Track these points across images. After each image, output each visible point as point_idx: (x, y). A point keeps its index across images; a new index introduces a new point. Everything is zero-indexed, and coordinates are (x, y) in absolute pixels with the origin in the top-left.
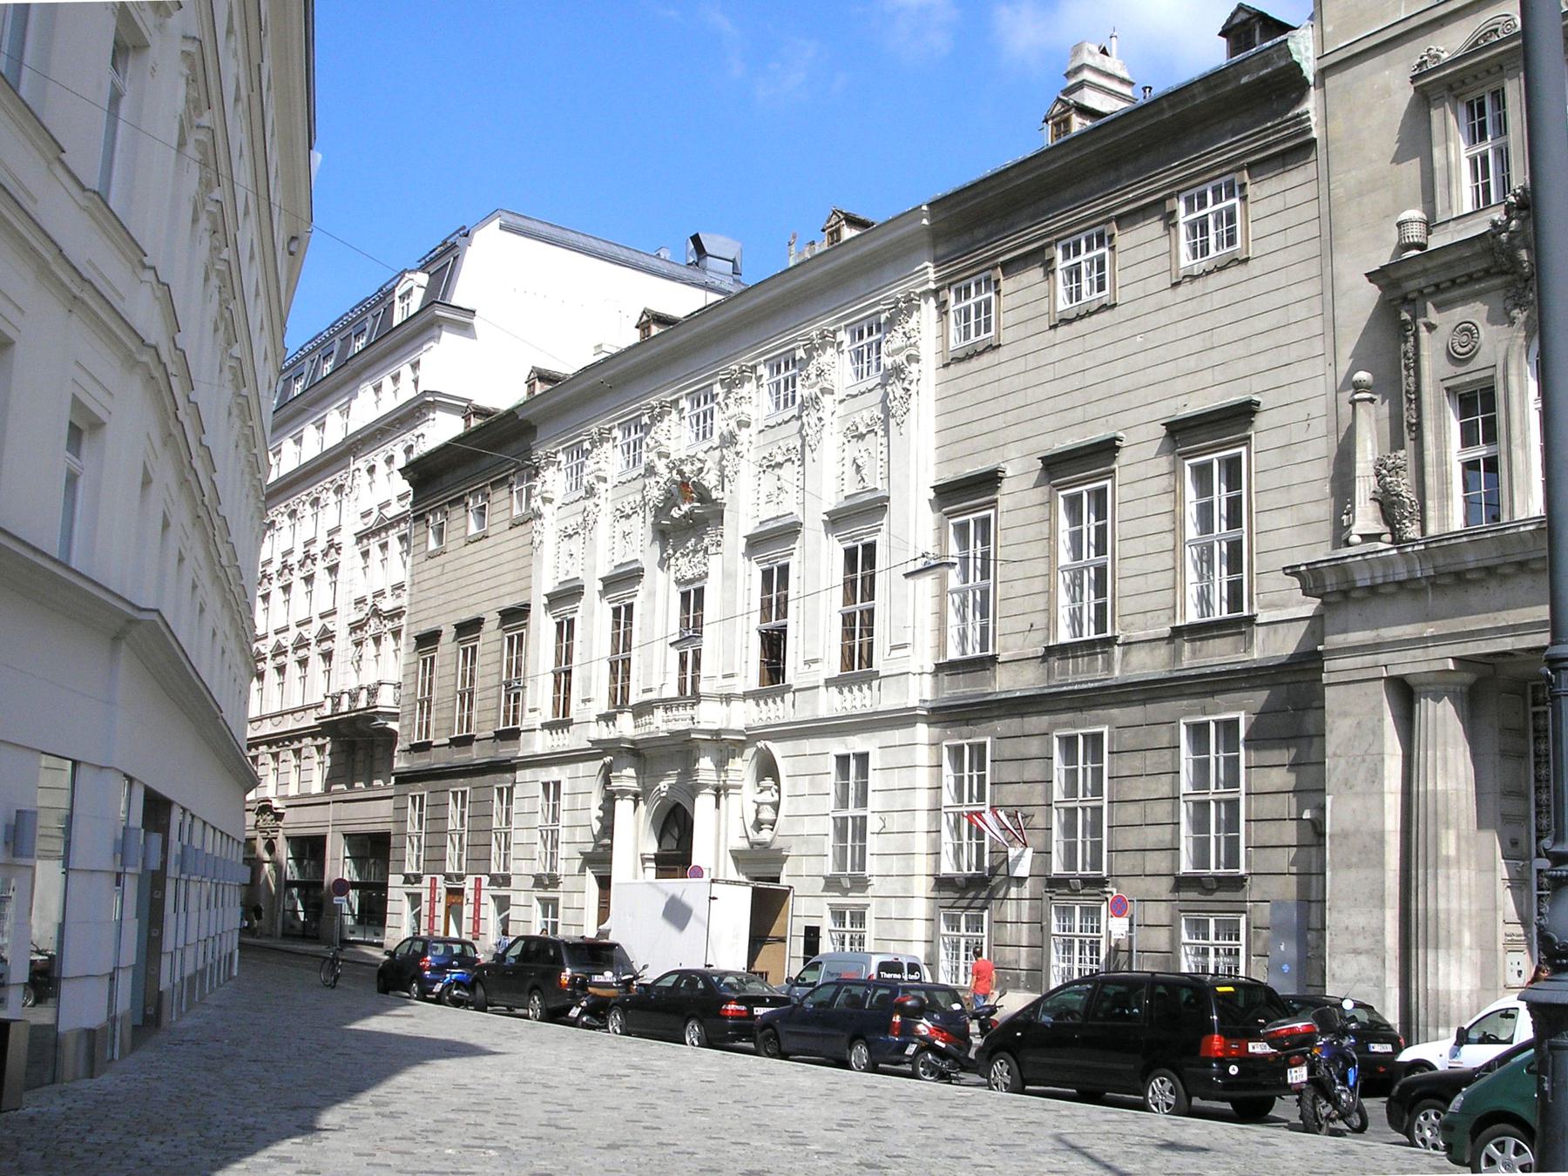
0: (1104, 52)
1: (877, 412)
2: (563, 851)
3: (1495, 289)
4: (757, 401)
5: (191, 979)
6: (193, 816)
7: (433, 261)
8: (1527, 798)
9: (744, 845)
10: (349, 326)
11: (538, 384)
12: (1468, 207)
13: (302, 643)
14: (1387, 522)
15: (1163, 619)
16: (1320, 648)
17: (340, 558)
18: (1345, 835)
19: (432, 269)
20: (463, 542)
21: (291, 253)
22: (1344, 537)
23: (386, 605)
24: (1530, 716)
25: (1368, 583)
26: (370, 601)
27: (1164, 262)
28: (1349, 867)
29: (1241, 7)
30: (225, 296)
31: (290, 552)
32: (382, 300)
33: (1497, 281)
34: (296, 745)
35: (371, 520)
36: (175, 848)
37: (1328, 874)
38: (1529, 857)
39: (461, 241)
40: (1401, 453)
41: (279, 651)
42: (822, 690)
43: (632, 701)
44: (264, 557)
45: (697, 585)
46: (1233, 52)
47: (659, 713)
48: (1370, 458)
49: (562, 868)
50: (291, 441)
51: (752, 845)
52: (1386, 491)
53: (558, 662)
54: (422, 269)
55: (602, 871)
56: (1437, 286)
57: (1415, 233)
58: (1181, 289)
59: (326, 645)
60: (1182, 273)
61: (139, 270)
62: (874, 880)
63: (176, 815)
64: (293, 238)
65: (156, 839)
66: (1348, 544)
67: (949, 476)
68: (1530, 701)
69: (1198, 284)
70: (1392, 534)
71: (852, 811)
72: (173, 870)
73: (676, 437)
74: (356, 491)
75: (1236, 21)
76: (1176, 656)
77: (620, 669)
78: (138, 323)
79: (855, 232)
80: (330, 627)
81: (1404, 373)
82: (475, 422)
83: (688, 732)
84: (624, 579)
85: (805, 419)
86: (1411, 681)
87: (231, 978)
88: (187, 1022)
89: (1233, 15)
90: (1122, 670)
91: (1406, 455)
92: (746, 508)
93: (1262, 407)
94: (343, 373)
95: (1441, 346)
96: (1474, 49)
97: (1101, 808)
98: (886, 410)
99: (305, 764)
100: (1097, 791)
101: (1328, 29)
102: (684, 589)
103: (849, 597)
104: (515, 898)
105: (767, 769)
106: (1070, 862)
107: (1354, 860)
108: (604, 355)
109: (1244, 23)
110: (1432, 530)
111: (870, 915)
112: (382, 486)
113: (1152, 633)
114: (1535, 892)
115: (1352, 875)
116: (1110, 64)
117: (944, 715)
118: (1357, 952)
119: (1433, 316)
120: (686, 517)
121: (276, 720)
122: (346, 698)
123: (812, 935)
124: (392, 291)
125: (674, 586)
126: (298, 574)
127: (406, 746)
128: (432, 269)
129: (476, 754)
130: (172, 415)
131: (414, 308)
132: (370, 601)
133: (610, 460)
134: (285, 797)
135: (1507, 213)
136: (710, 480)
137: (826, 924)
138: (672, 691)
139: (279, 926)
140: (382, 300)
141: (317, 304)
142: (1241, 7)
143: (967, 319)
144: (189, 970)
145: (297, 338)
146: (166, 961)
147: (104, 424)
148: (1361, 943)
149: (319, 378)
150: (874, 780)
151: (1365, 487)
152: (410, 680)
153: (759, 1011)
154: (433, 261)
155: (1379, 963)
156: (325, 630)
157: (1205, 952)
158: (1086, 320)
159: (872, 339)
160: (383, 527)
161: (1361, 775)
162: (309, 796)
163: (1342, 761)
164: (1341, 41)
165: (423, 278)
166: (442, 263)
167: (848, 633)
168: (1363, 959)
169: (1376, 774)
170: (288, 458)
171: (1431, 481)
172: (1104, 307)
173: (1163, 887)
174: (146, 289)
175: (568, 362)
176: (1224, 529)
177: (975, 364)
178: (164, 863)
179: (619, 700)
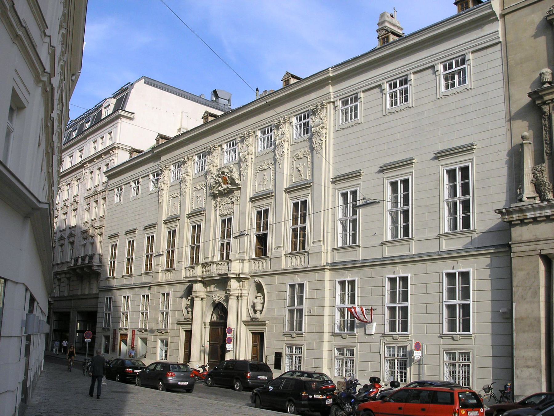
0: (392, 16)
1: (308, 150)
2: (170, 320)
7: (118, 95)
10: (86, 117)
11: (161, 140)
14: (537, 193)
16: (510, 243)
18: (522, 319)
19: (118, 98)
20: (380, 115)
21: (72, 80)
23: (97, 224)
26: (90, 222)
27: (380, 108)
28: (524, 332)
35: (91, 192)
40: (544, 165)
41: (62, 238)
47: (214, 267)
48: (530, 166)
49: (169, 327)
50: (68, 157)
51: (252, 319)
52: (537, 179)
53: (193, 242)
54: (114, 97)
55: (188, 328)
64: (73, 75)
66: (521, 200)
70: (540, 197)
73: (221, 159)
77: (195, 249)
80: (73, 232)
82: (135, 155)
83: (227, 274)
92: (251, 185)
99: (62, 285)
105: (259, 288)
107: (527, 329)
108: (182, 132)
112: (96, 179)
118: (528, 367)
120: (225, 188)
121: (60, 266)
124: (102, 106)
125: (218, 217)
126: (70, 209)
128: (118, 98)
131: (110, 112)
133: (192, 169)
134: (54, 297)
136: (236, 176)
137: (286, 351)
147: (25, 107)
148: (530, 363)
149: (71, 138)
151: (528, 178)
154: (118, 95)
157: (454, 365)
159: (305, 121)
162: (64, 297)
163: (520, 289)
165: (114, 101)
167: (295, 236)
168: (532, 370)
169: (536, 293)
170: (67, 165)
175: (172, 134)
179: (195, 260)
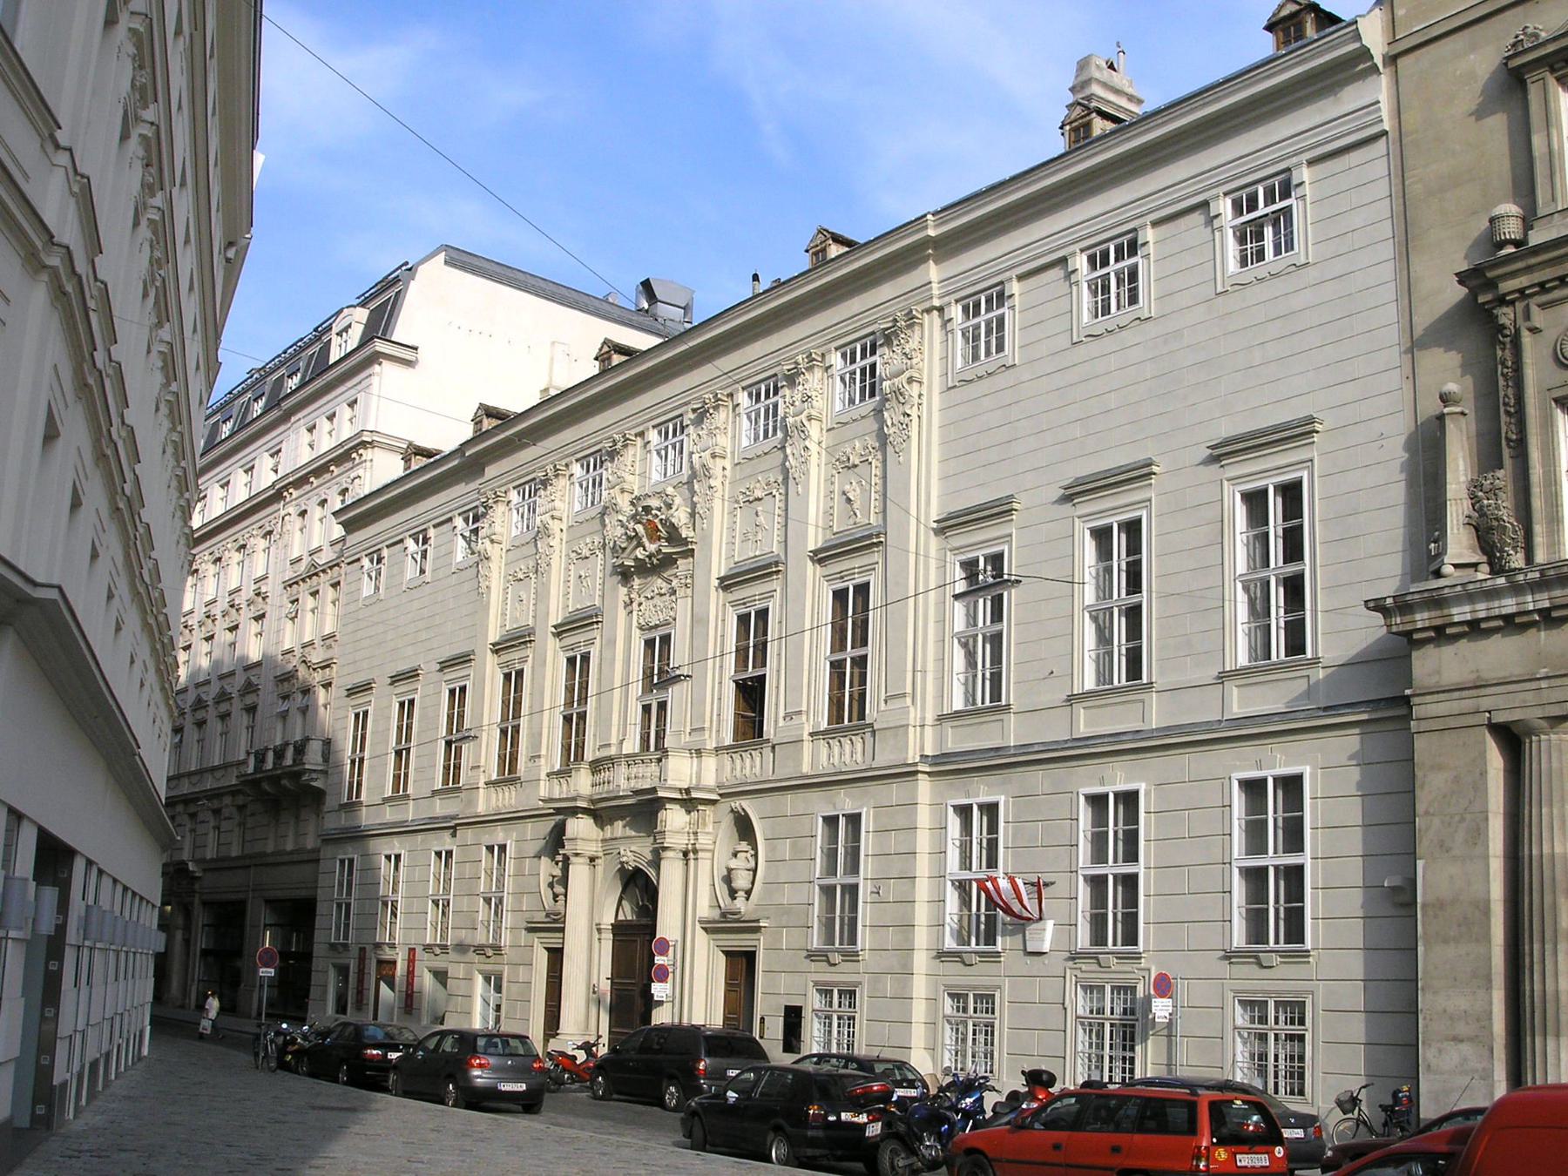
0: (1111, 67)
1: (872, 442)
2: (508, 920)
4: (733, 433)
5: (94, 1065)
6: (101, 872)
10: (287, 360)
13: (223, 697)
14: (1484, 551)
16: (1408, 692)
17: (268, 609)
18: (1441, 905)
19: (373, 305)
21: (228, 260)
22: (1433, 567)
26: (298, 652)
28: (1446, 941)
30: (157, 254)
32: (318, 338)
35: (302, 567)
36: (77, 907)
37: (1420, 949)
40: (1500, 473)
43: (589, 755)
44: (187, 607)
45: (662, 631)
47: (622, 770)
48: (1463, 479)
49: (506, 939)
52: (1482, 514)
54: (363, 305)
55: (553, 940)
57: (1512, 229)
59: (249, 700)
60: (1229, 282)
61: (50, 148)
63: (79, 865)
64: (231, 244)
65: (50, 894)
70: (1490, 563)
72: (72, 936)
73: (644, 470)
75: (1285, 13)
77: (574, 722)
78: (49, 218)
81: (1501, 379)
83: (654, 790)
84: (579, 622)
85: (788, 451)
87: (140, 1059)
88: (91, 1119)
91: (1504, 477)
94: (275, 414)
95: (1547, 352)
98: (883, 439)
101: (1400, 12)
102: (649, 636)
103: (839, 643)
105: (744, 828)
109: (1293, 15)
110: (1540, 557)
111: (1002, 1000)
112: (313, 530)
115: (1451, 951)
116: (1116, 79)
118: (1457, 1039)
119: (1539, 318)
121: (195, 779)
123: (793, 1017)
124: (330, 328)
125: (636, 633)
128: (373, 305)
130: (87, 356)
131: (353, 343)
132: (298, 652)
133: (566, 499)
136: (680, 516)
138: (632, 745)
140: (318, 338)
141: (252, 339)
144: (92, 1053)
145: (231, 376)
146: (61, 1050)
148: (1462, 1029)
150: (867, 843)
155: (1486, 1053)
157: (1263, 1038)
160: (314, 572)
161: (1460, 836)
163: (1436, 821)
164: (1413, 26)
165: (362, 315)
166: (383, 302)
168: (1465, 1048)
169: (1478, 833)
170: (214, 504)
171: (1537, 503)
174: (59, 175)
175: (517, 400)
176: (1281, 563)
178: (61, 929)
179: (573, 752)
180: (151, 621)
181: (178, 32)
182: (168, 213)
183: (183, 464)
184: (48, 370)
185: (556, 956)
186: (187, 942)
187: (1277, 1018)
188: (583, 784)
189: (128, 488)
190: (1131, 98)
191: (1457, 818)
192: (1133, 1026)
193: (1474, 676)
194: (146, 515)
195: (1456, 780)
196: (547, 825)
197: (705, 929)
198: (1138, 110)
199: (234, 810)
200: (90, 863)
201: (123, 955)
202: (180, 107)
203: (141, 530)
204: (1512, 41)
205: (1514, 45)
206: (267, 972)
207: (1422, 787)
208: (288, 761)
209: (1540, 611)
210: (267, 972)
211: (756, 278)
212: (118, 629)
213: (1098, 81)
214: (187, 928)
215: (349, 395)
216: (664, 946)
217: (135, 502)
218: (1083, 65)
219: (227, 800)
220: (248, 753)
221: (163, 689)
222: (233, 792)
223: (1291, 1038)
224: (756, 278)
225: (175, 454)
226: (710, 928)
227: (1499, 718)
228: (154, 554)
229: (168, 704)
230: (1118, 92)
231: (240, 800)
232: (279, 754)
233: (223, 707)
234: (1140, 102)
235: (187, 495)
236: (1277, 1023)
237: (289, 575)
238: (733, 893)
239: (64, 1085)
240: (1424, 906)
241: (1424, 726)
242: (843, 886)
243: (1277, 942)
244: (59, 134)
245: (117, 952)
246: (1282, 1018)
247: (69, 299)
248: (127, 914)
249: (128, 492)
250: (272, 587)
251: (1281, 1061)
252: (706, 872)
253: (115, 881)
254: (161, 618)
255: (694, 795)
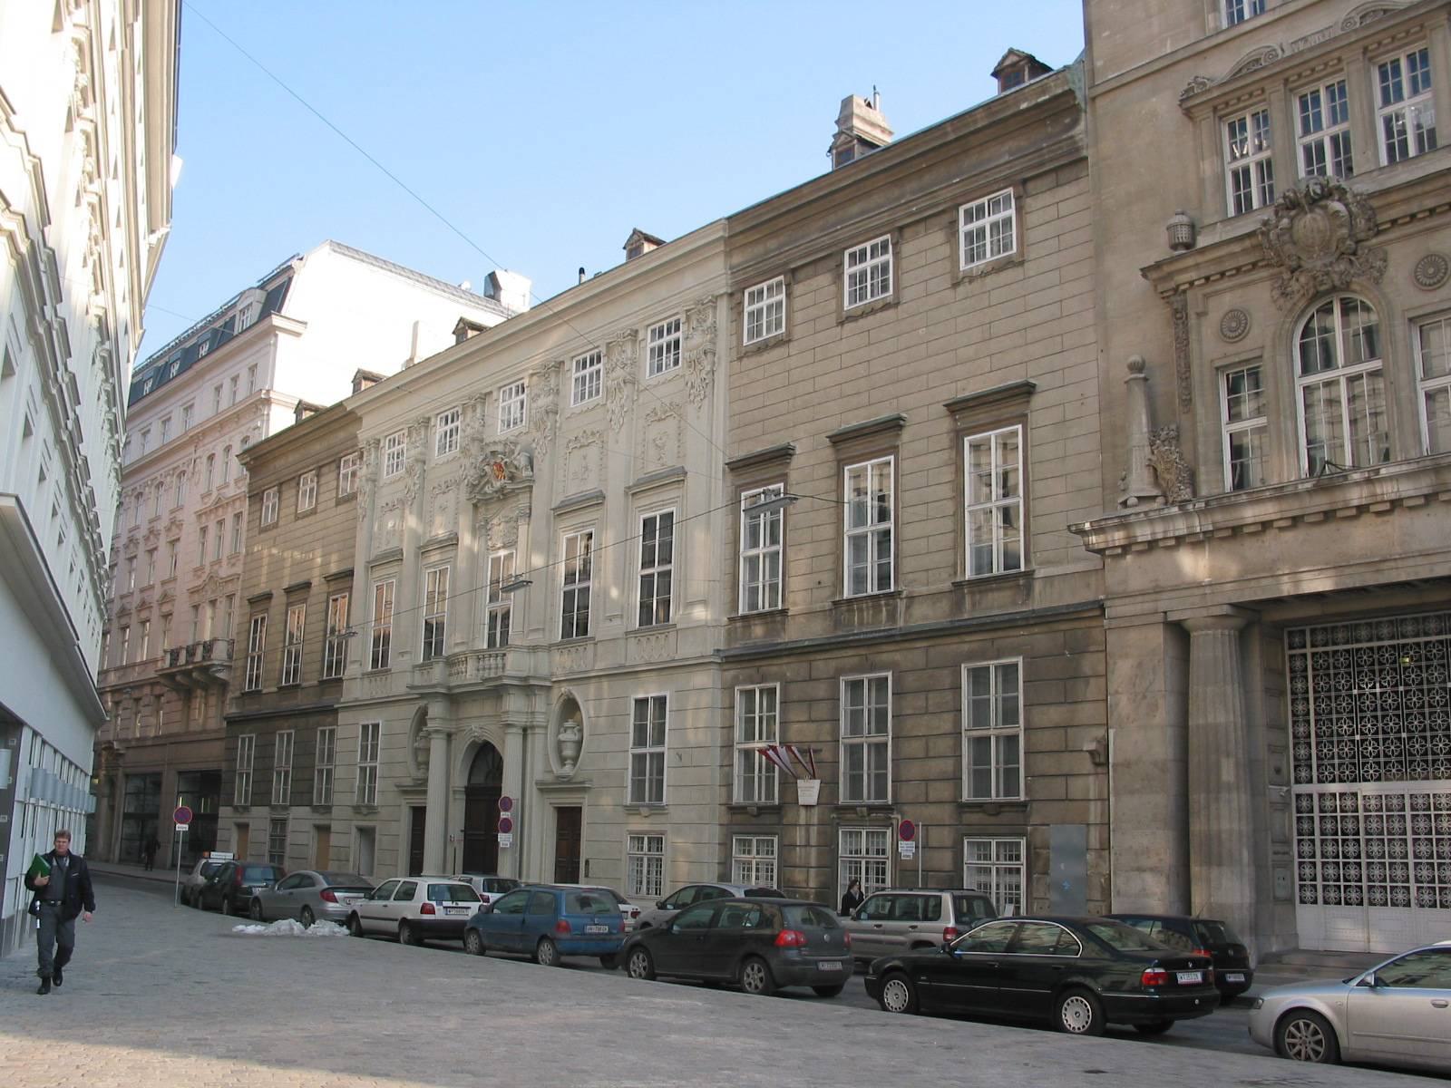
3: (1262, 280)
6: (44, 742)
8: (1284, 729)
9: (549, 778)
12: (1233, 214)
13: (144, 606)
15: (944, 576)
24: (1287, 658)
25: (1149, 538)
28: (1132, 792)
29: (1011, 52)
31: (157, 518)
33: (1264, 273)
34: (136, 694)
36: (24, 771)
38: (1288, 784)
39: (295, 263)
42: (622, 642)
46: (1004, 87)
55: (416, 801)
56: (1207, 279)
58: (961, 289)
60: (961, 275)
62: (671, 809)
63: (26, 735)
67: (741, 453)
68: (1286, 646)
69: (977, 285)
71: (368, 764)
74: (197, 476)
75: (1008, 62)
76: (958, 605)
79: (476, 333)
83: (500, 678)
86: (1189, 624)
89: (1005, 58)
90: (905, 621)
93: (1038, 389)
96: (1237, 75)
97: (1016, 737)
100: (881, 727)
104: (335, 826)
106: (855, 790)
109: (1014, 65)
113: (933, 588)
114: (1295, 815)
117: (730, 660)
122: (200, 651)
126: (142, 548)
127: (238, 694)
129: (302, 701)
135: (1276, 213)
139: (117, 852)
142: (1011, 52)
143: (584, 384)
152: (243, 637)
153: (1184, 978)
156: (165, 595)
157: (988, 871)
158: (871, 318)
172: (887, 306)
173: (945, 813)
175: (388, 366)
177: (766, 357)
180: (87, 537)
181: (112, 47)
182: (102, 200)
183: (114, 410)
184: (40, 454)
185: (419, 814)
186: (112, 808)
187: (998, 856)
188: (437, 673)
189: (70, 424)
190: (884, 130)
191: (1140, 697)
192: (884, 863)
193: (1154, 584)
194: (84, 449)
195: (1140, 665)
196: (410, 711)
197: (539, 789)
198: (890, 140)
199: (152, 698)
200: (35, 734)
201: (60, 814)
202: (113, 112)
203: (80, 462)
204: (1186, 87)
205: (1186, 91)
206: (182, 827)
207: (1113, 672)
208: (198, 657)
209: (1204, 533)
210: (182, 827)
211: (582, 271)
212: (60, 541)
213: (858, 117)
214: (112, 796)
215: (250, 362)
216: (508, 804)
217: (76, 437)
218: (847, 103)
219: (147, 690)
220: (165, 652)
221: (96, 595)
222: (153, 684)
223: (1010, 871)
224: (582, 271)
225: (108, 402)
226: (544, 789)
227: (1173, 617)
228: (89, 483)
229: (99, 609)
230: (873, 124)
231: (158, 690)
232: (191, 652)
233: (144, 615)
234: (891, 133)
235: (116, 436)
236: (998, 859)
237: (199, 507)
238: (563, 761)
239: (11, 920)
240: (1114, 765)
241: (1114, 623)
242: (652, 755)
243: (997, 795)
244: (13, 118)
245: (56, 811)
246: (1002, 857)
247: (65, 447)
248: (65, 776)
249: (70, 427)
250: (188, 517)
251: (1002, 891)
252: (541, 744)
253: (56, 751)
254: (95, 537)
255: (532, 682)
